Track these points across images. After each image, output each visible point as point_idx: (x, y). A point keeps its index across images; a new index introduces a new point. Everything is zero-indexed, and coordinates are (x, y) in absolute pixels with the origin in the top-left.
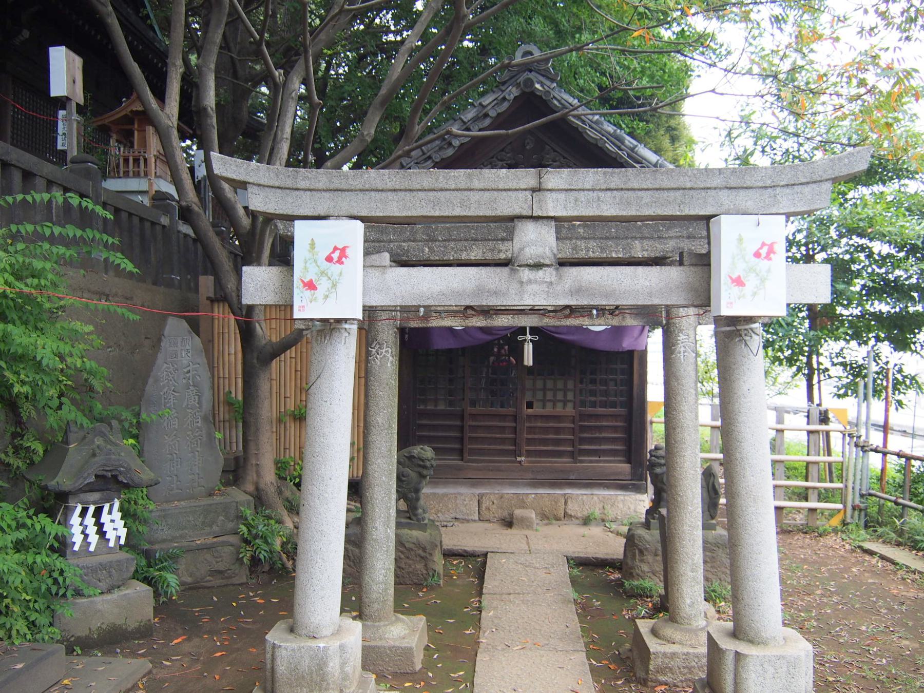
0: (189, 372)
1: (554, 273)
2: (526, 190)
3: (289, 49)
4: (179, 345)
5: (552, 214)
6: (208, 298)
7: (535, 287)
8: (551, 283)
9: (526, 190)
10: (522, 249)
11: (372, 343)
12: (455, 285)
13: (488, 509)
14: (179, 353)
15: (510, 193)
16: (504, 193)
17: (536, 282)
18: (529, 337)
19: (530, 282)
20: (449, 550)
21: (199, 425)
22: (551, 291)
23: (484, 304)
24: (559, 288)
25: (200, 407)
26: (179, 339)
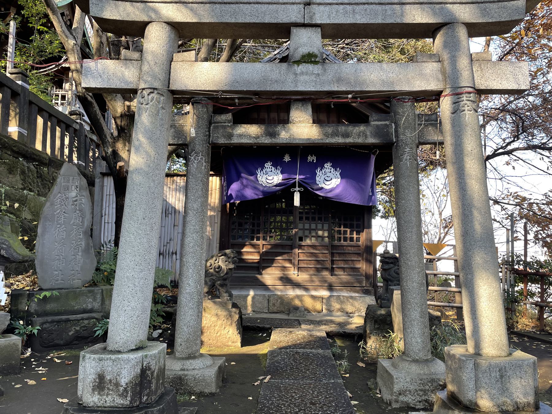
0: (76, 201)
1: (321, 67)
2: (299, 3)
3: (184, 146)
4: (71, 181)
5: (319, 22)
6: (101, 173)
7: (306, 78)
8: (318, 75)
9: (299, 3)
10: (296, 49)
11: (192, 152)
12: (246, 76)
13: (274, 305)
14: (70, 187)
15: (288, 6)
16: (283, 6)
17: (307, 74)
18: (297, 189)
19: (302, 73)
20: (248, 326)
21: (81, 237)
22: (318, 80)
23: (268, 89)
24: (324, 78)
25: (83, 225)
26: (71, 178)
